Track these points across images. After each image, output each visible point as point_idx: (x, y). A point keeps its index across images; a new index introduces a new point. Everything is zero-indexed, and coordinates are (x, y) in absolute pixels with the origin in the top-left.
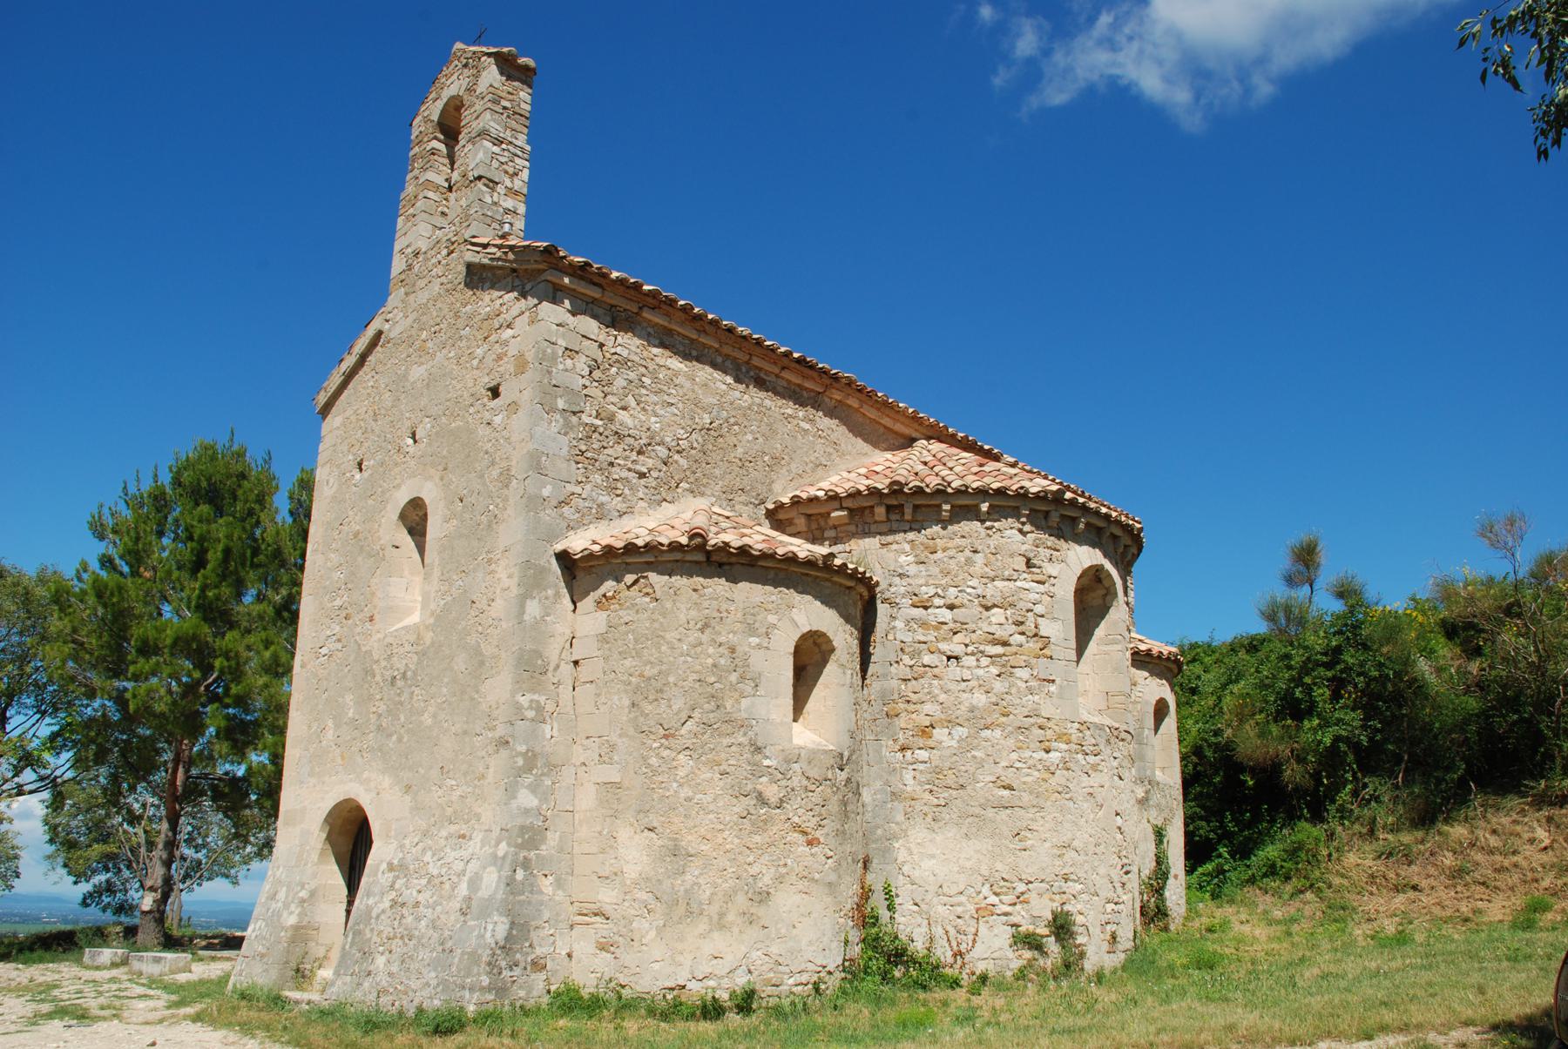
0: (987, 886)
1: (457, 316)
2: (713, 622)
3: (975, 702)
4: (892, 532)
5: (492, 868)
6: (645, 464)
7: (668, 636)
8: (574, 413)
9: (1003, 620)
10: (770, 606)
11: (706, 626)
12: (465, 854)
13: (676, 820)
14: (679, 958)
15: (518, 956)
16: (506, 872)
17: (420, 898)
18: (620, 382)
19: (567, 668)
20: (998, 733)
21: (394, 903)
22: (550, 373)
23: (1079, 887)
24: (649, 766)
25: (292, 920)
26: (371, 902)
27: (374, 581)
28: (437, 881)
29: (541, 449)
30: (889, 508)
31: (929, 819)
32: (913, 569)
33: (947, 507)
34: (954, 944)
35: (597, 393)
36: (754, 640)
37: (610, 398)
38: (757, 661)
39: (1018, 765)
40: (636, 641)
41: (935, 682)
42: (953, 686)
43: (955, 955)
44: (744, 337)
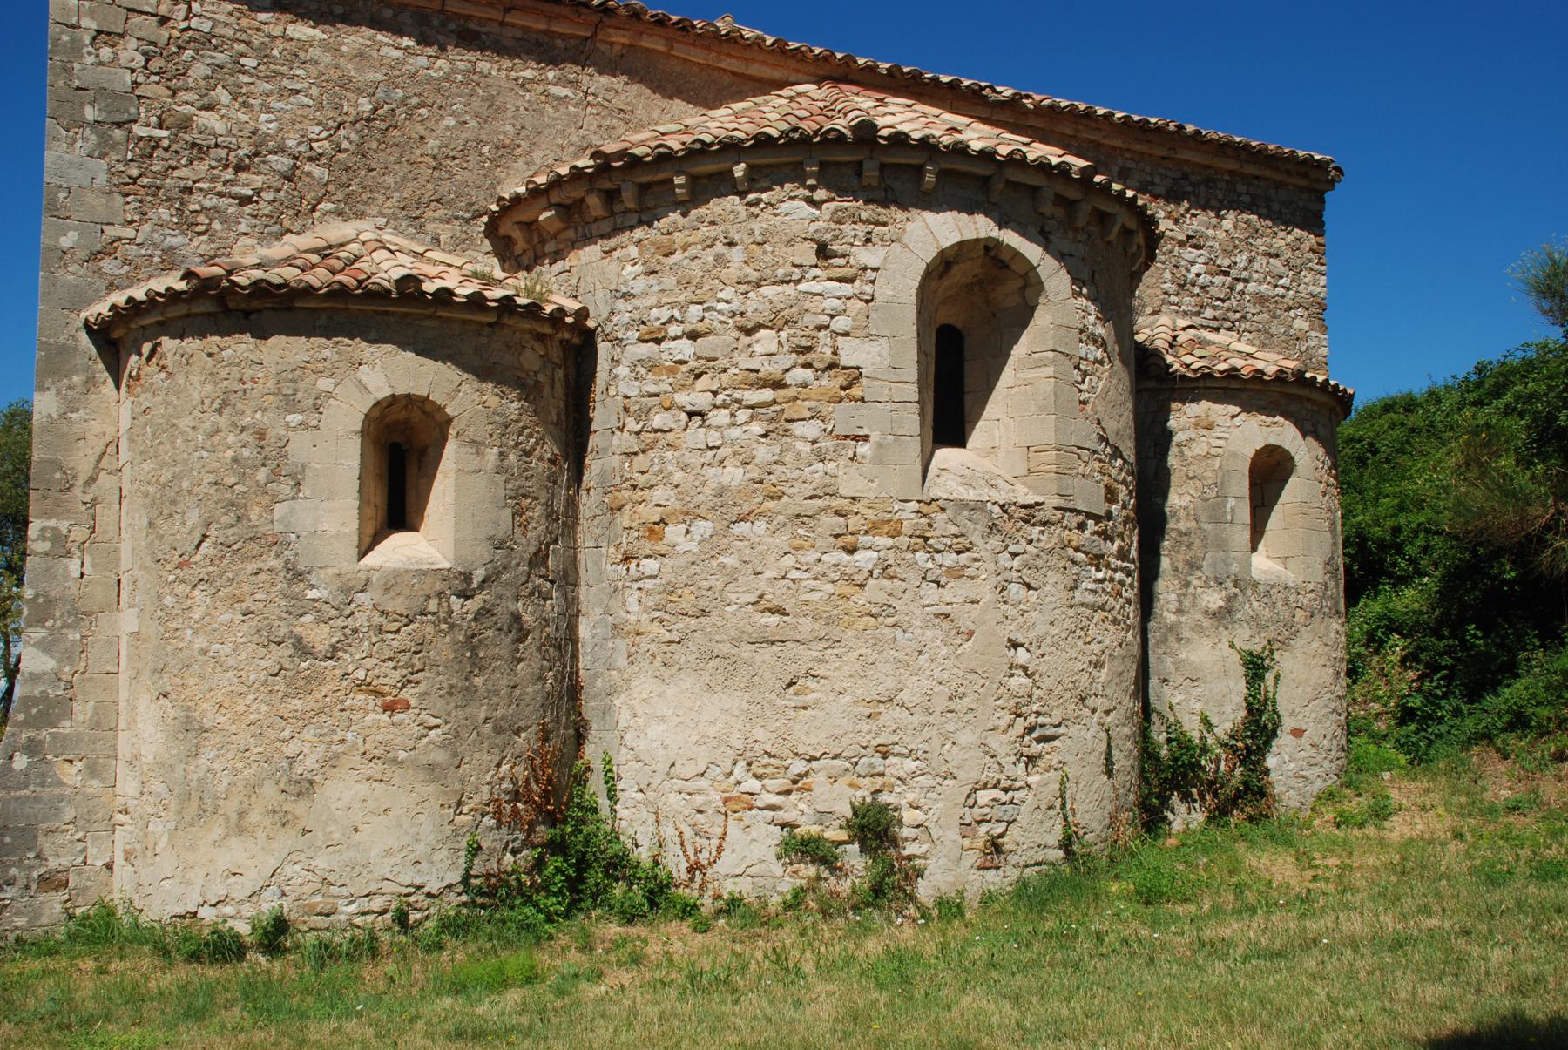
0: (742, 764)
2: (233, 399)
3: (725, 481)
4: (617, 231)
8: (119, 125)
9: (773, 348)
11: (225, 404)
14: (191, 875)
15: (13, 871)
18: (199, 71)
20: (761, 526)
23: (910, 765)
31: (657, 663)
33: (679, 180)
34: (691, 852)
36: (295, 419)
37: (184, 96)
38: (300, 448)
39: (794, 574)
41: (669, 454)
42: (695, 459)
43: (690, 870)
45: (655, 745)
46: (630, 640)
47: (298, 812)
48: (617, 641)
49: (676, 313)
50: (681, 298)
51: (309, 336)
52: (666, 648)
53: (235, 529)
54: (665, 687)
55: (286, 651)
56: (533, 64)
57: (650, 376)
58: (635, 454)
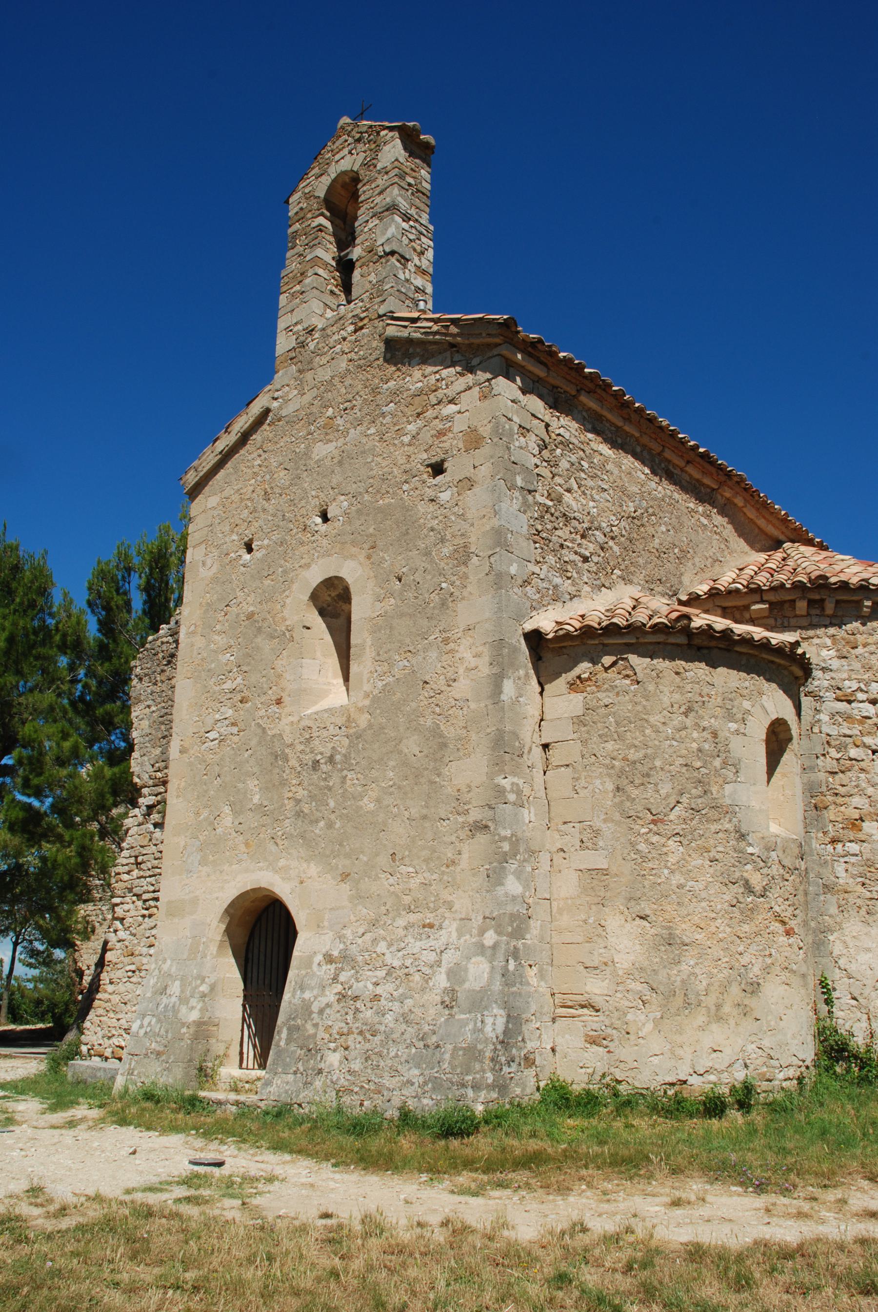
1: (375, 391)
2: (696, 707)
5: (480, 958)
6: (589, 547)
7: (652, 719)
8: (530, 492)
10: (745, 692)
11: (689, 710)
12: (439, 945)
13: (668, 908)
14: (680, 1052)
16: (499, 962)
17: (379, 990)
19: (538, 751)
21: (342, 997)
22: (509, 448)
24: (638, 851)
25: (194, 1016)
26: (307, 995)
27: (279, 663)
28: (401, 973)
29: (508, 526)
30: (811, 603)
31: (863, 912)
32: (835, 664)
33: (868, 603)
35: (546, 473)
36: (733, 726)
37: (558, 480)
38: (736, 745)
40: (617, 724)
41: (862, 775)
44: (661, 428)
45: (864, 967)
46: (841, 897)
47: (752, 1006)
48: (829, 896)
49: (863, 686)
50: (866, 677)
51: (739, 671)
52: (869, 903)
53: (702, 800)
54: (870, 928)
55: (739, 889)
56: (693, 500)
57: (845, 723)
58: (836, 773)
